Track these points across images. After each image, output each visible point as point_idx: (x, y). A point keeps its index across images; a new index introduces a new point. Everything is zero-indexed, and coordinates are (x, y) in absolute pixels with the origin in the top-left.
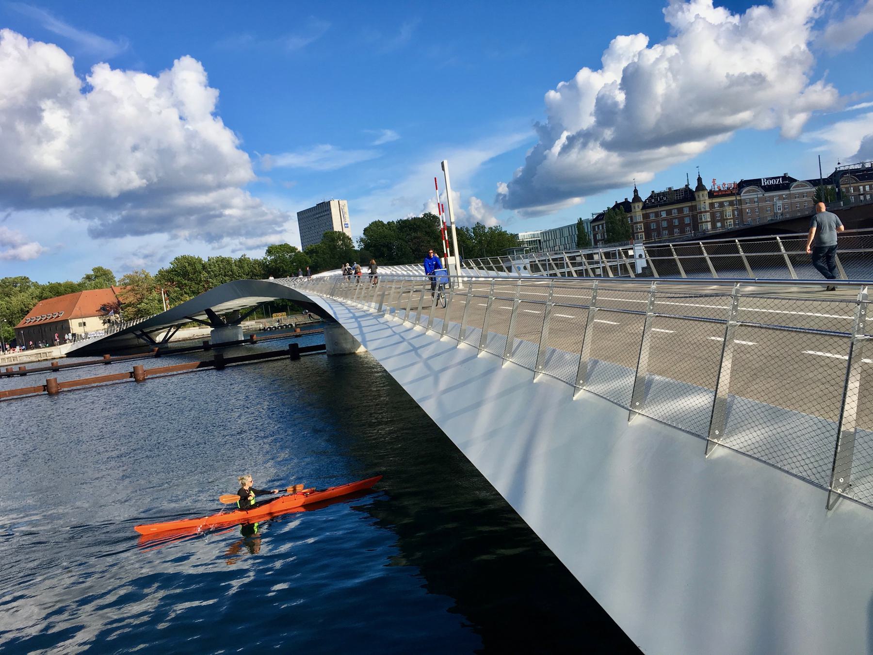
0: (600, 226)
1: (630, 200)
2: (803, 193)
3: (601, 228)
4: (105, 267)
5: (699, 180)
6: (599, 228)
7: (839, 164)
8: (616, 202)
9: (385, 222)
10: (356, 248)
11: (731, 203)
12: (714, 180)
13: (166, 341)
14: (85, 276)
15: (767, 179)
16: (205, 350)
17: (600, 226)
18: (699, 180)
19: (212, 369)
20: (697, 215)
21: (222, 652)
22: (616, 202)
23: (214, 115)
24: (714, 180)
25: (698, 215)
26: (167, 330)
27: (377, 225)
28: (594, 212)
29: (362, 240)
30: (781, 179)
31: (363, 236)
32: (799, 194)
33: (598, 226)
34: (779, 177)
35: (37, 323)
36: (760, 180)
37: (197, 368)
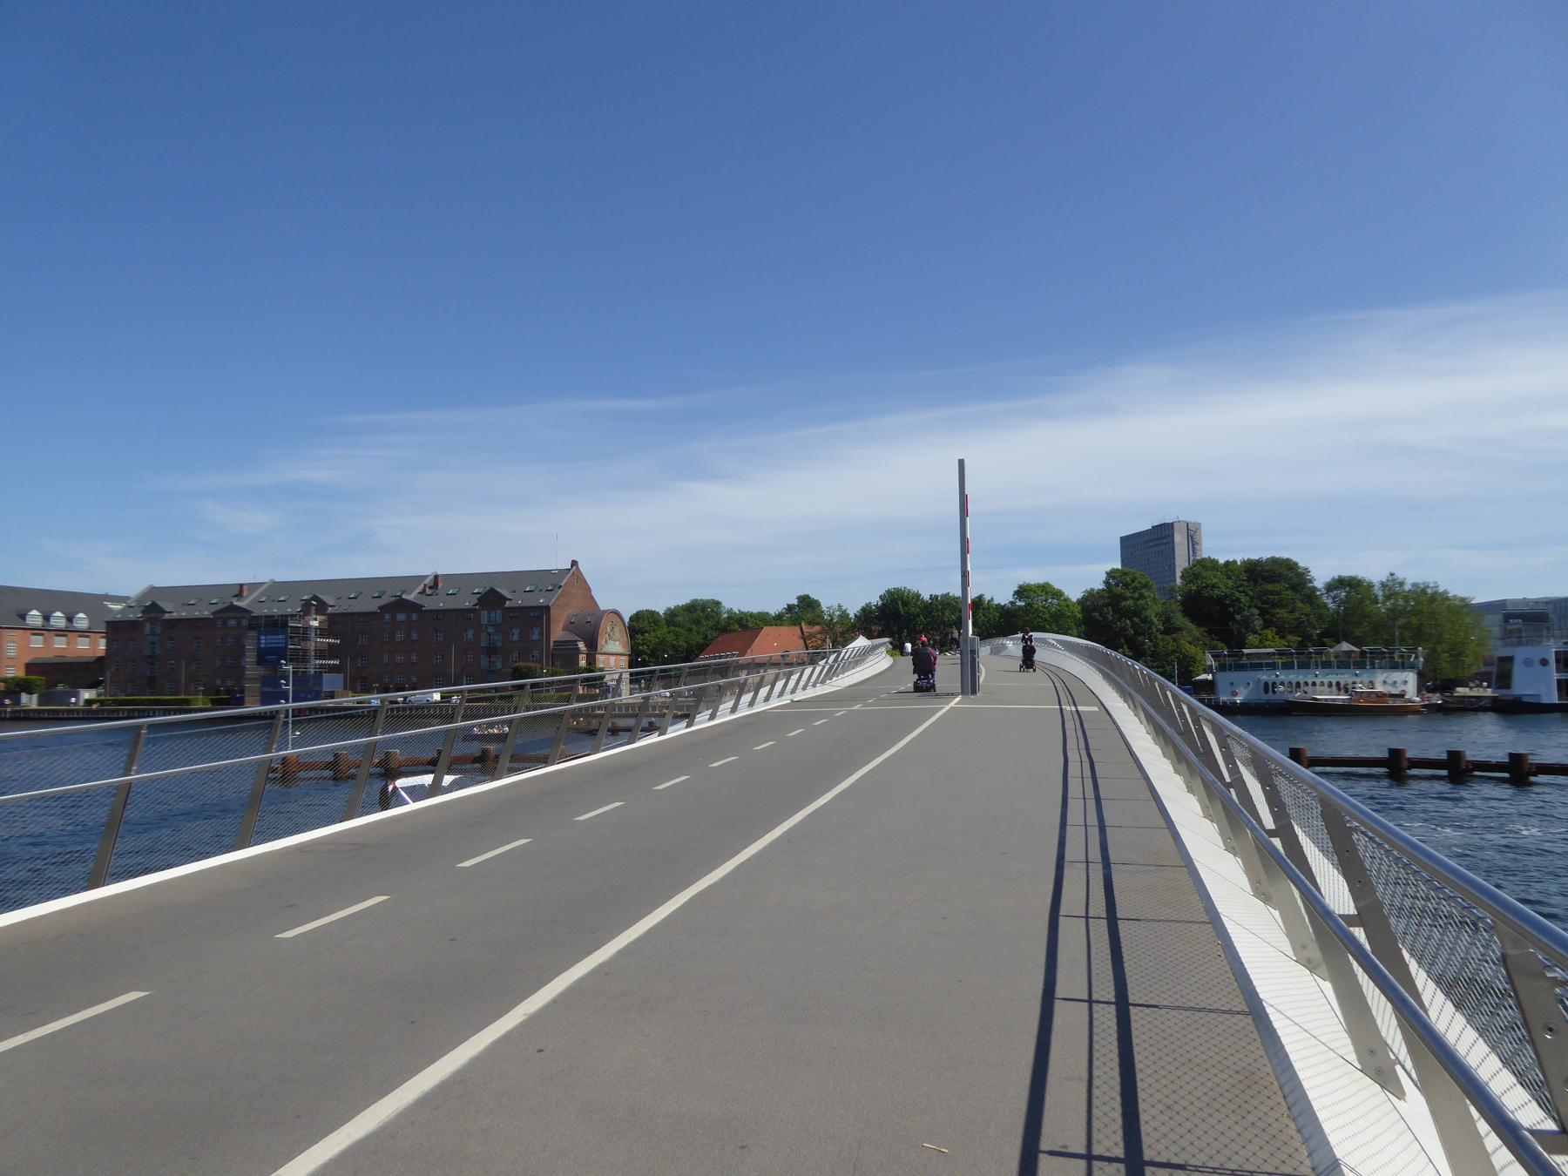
4: (814, 596)
9: (1222, 561)
31: (996, 602)
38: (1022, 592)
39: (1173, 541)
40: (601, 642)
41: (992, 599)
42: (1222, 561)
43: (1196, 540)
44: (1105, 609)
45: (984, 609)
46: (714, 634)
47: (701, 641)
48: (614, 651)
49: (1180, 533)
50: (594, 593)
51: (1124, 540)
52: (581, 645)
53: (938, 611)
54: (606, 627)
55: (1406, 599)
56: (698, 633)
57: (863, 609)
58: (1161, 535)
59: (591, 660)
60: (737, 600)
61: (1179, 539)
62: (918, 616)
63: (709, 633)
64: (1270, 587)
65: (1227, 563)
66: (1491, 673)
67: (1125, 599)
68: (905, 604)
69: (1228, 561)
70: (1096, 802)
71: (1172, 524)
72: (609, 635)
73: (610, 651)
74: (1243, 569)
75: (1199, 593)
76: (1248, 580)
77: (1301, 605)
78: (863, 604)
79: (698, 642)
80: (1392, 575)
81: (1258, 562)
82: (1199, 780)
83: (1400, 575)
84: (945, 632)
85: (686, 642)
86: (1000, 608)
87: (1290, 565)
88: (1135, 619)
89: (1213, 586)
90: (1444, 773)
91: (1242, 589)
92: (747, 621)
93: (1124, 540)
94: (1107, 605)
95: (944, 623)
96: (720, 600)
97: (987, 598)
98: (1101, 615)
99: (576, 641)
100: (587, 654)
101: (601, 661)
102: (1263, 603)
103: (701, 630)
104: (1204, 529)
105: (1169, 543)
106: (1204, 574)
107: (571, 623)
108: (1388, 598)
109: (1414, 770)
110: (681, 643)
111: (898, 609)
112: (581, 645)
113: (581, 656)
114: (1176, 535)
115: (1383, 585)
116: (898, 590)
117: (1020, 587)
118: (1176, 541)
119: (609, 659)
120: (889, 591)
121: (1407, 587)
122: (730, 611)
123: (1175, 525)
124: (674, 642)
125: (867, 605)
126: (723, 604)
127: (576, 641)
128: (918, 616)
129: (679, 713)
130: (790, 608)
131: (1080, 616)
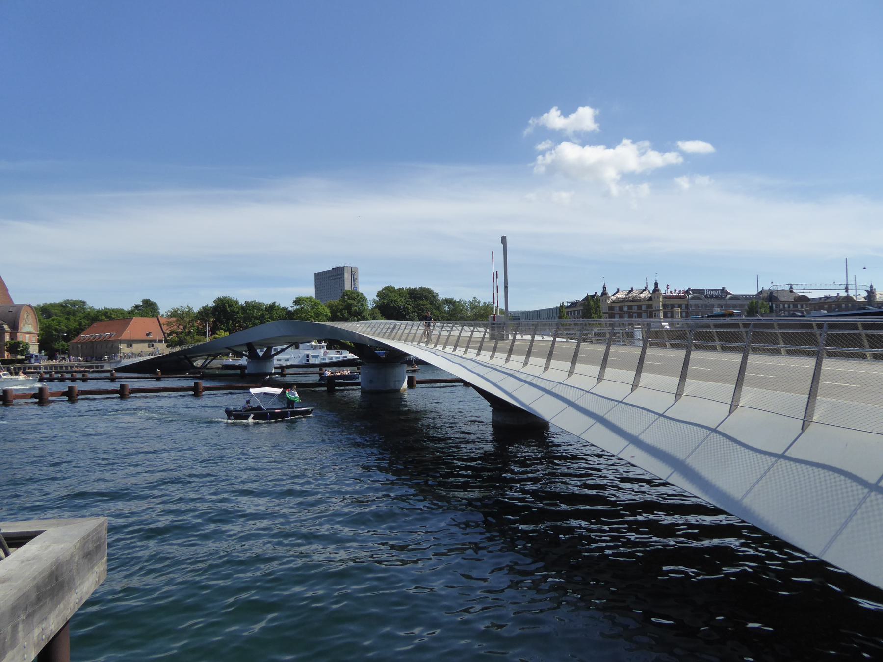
0: (569, 313)
1: (599, 294)
2: (735, 305)
3: (573, 314)
4: (153, 300)
5: (656, 285)
6: (571, 314)
7: (772, 283)
8: (587, 294)
9: (396, 288)
10: (353, 309)
11: (680, 306)
12: (668, 285)
13: (204, 367)
14: (134, 306)
15: (709, 290)
16: (72, 381)
17: (569, 313)
18: (656, 285)
19: (117, 397)
20: (652, 313)
21: (765, 544)
22: (587, 294)
23: (583, 147)
24: (668, 285)
25: (654, 312)
26: (206, 357)
27: (389, 290)
28: (568, 301)
29: (375, 301)
30: (720, 291)
31: (159, 311)
32: (733, 304)
33: (575, 312)
34: (719, 290)
35: (405, 322)
36: (704, 290)
37: (61, 396)
38: (297, 301)
39: (344, 277)
40: (21, 325)
41: (279, 304)
42: (396, 288)
43: (356, 277)
44: (343, 311)
45: (275, 310)
46: (87, 322)
47: (77, 326)
48: (29, 331)
49: (348, 272)
50: (10, 293)
51: (317, 275)
52: (6, 327)
53: (250, 310)
54: (24, 315)
55: (481, 309)
56: (75, 321)
57: (204, 308)
58: (337, 273)
59: (13, 336)
60: (97, 302)
61: (347, 276)
62: (238, 313)
63: (83, 321)
64: (421, 302)
65: (400, 289)
66: (4, 357)
67: (354, 306)
68: (230, 306)
69: (400, 288)
70: (548, 394)
71: (343, 267)
72: (26, 321)
73: (26, 331)
74: (407, 293)
75: (388, 304)
76: (410, 298)
77: (435, 311)
78: (204, 306)
79: (75, 327)
80: (474, 298)
81: (415, 290)
82: (471, 387)
83: (478, 298)
84: (254, 322)
85: (66, 327)
86: (285, 309)
87: (430, 292)
88: (359, 317)
89: (395, 301)
90: (118, 395)
91: (408, 303)
92: (111, 314)
93: (317, 275)
94: (344, 309)
95: (253, 317)
96: (86, 301)
97: (277, 304)
98: (341, 315)
99: (3, 324)
100: (10, 333)
101: (20, 337)
102: (418, 310)
103: (77, 319)
104: (359, 271)
105: (341, 277)
106: (390, 294)
107: (10, 312)
108: (472, 309)
109: (205, 392)
110: (63, 327)
111: (226, 309)
112: (6, 327)
113: (6, 334)
114: (345, 274)
115: (471, 303)
116: (224, 298)
117: (297, 298)
118: (345, 277)
119: (25, 337)
120: (219, 298)
121: (481, 304)
122: (92, 308)
123: (345, 268)
124: (58, 327)
125: (206, 306)
126: (87, 303)
127: (3, 324)
128: (238, 313)
129: (91, 370)
130: (137, 307)
131: (330, 315)
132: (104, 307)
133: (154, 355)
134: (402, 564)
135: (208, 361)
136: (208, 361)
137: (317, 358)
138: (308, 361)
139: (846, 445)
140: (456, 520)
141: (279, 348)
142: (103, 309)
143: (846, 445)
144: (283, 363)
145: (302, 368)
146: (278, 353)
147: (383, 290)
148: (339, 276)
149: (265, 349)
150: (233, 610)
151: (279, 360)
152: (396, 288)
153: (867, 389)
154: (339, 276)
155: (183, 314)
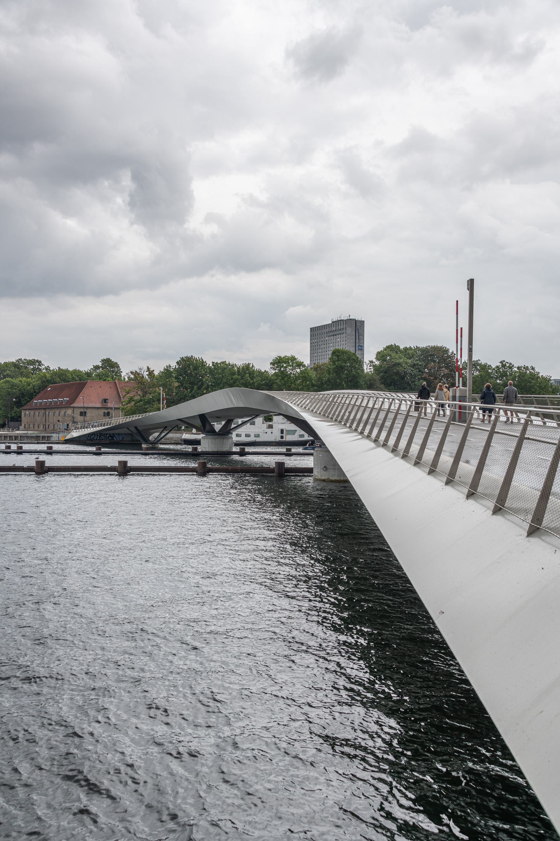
4: (114, 360)
42: (209, 363)
65: (406, 349)
132: (59, 368)
133: (104, 426)
134: (385, 815)
135: (163, 434)
136: (163, 434)
137: (294, 434)
138: (282, 437)
139: (541, 712)
140: (61, 773)
141: (240, 421)
142: (57, 369)
143: (541, 712)
144: (243, 439)
145: (275, 446)
146: (239, 426)
147: (385, 349)
148: (340, 332)
149: (223, 423)
150: (462, 839)
151: (237, 435)
152: (402, 347)
153: (319, 605)
154: (340, 332)
155: (225, 369)
